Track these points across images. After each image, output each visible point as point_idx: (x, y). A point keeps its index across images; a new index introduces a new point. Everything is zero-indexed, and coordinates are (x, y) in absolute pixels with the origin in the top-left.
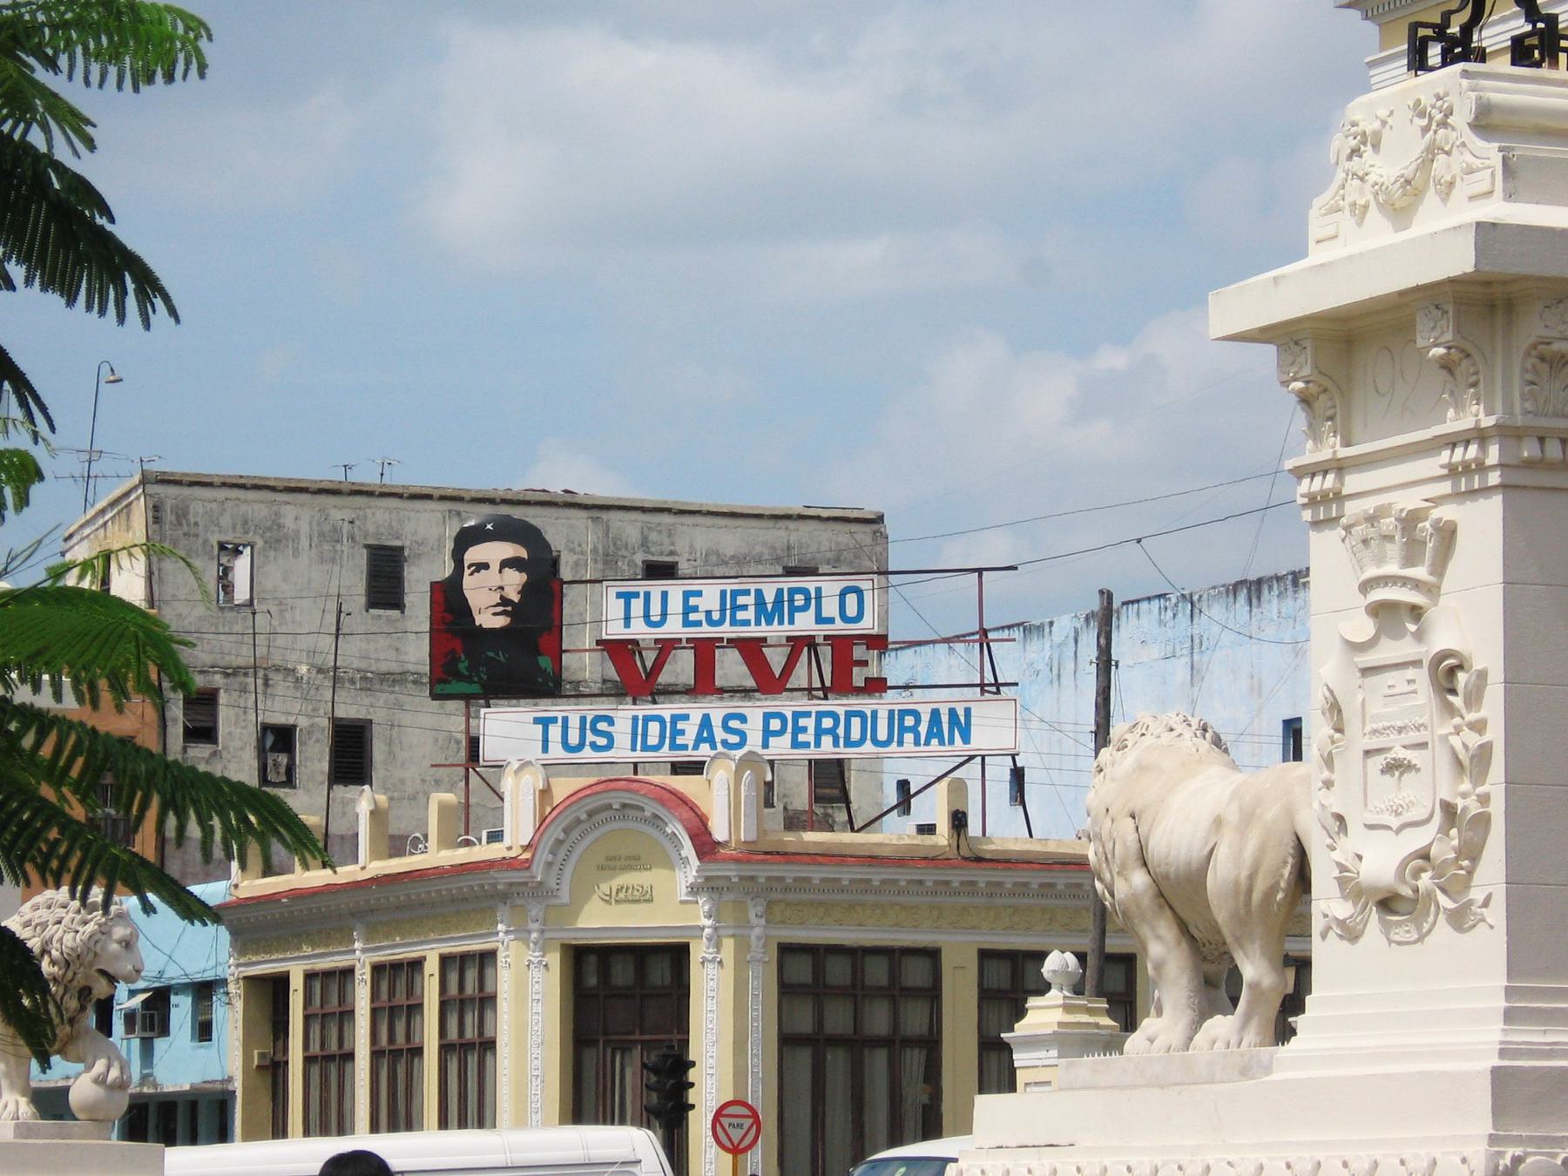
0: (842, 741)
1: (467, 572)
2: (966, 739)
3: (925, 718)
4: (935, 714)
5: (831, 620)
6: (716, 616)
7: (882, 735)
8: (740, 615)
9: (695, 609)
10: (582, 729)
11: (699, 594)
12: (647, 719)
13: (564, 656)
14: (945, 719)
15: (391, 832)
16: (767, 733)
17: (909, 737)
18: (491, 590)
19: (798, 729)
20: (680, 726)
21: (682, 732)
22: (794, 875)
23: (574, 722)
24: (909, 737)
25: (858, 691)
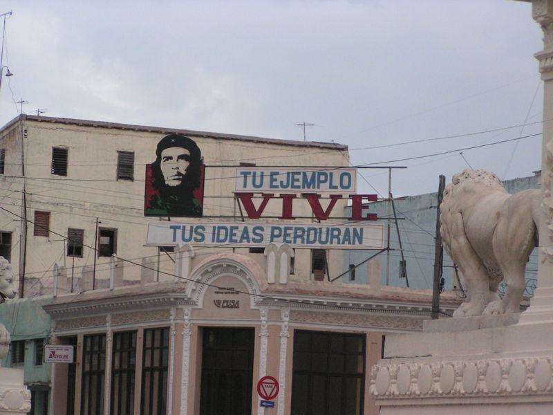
0: (305, 241)
1: (163, 160)
2: (360, 242)
3: (343, 232)
4: (347, 230)
5: (336, 187)
6: (285, 184)
7: (323, 239)
8: (296, 184)
9: (276, 180)
10: (191, 231)
11: (277, 174)
12: (220, 228)
13: (204, 199)
14: (352, 235)
15: (124, 279)
16: (273, 236)
17: (335, 240)
18: (172, 171)
19: (286, 235)
20: (234, 231)
21: (235, 235)
22: (400, 305)
23: (188, 228)
24: (335, 240)
25: (364, 219)
